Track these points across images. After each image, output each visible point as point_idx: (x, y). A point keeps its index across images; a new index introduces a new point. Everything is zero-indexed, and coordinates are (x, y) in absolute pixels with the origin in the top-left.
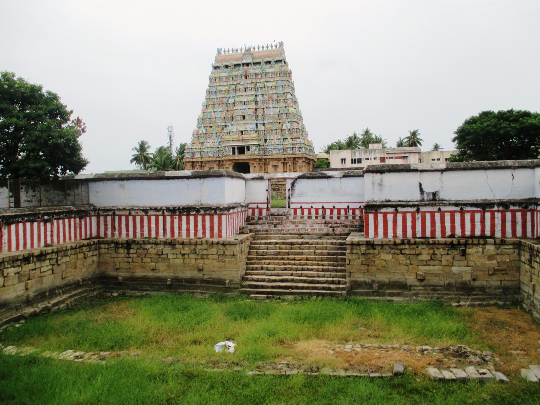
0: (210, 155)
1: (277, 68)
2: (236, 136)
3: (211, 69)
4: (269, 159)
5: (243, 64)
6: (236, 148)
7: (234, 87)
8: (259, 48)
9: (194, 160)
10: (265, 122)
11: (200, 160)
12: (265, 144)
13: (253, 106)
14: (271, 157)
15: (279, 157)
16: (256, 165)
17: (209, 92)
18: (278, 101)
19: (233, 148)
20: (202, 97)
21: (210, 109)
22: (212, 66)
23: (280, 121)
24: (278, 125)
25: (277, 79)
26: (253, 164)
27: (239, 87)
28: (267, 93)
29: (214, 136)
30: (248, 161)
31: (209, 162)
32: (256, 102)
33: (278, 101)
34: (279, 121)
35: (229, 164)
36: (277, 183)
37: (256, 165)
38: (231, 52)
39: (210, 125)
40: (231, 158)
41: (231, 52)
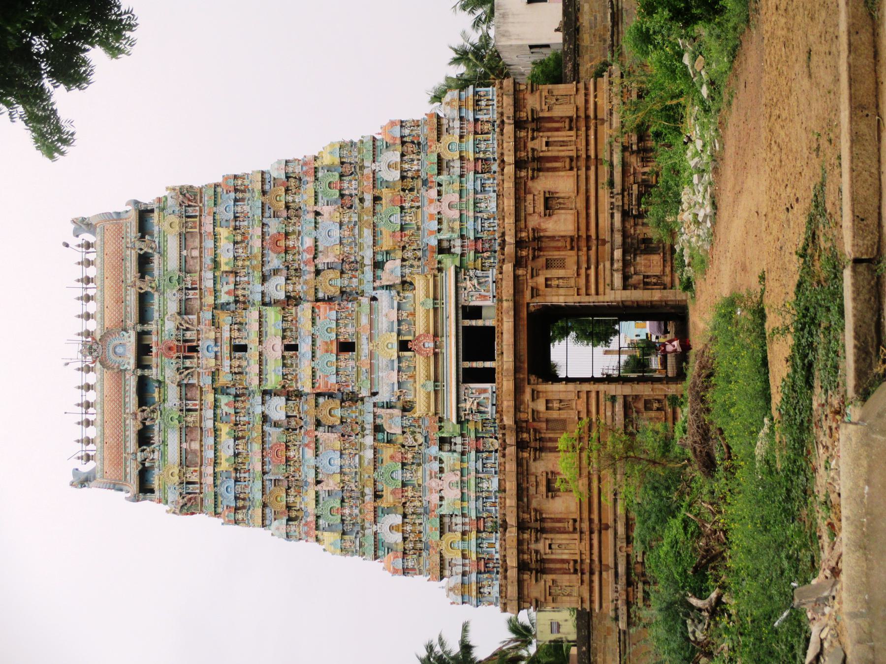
0: (494, 485)
1: (167, 229)
2: (420, 361)
3: (148, 506)
4: (517, 231)
5: (141, 364)
6: (468, 365)
7: (224, 400)
8: (88, 316)
9: (512, 562)
10: (368, 261)
11: (512, 533)
12: (458, 250)
13: (304, 311)
14: (510, 221)
15: (509, 185)
16: (541, 280)
17: (238, 511)
18: (292, 211)
19: (469, 376)
20: (259, 545)
21: (307, 502)
22: (137, 500)
23: (368, 197)
24: (385, 206)
25: (208, 221)
26: (535, 292)
27: (225, 378)
28: (256, 262)
29: (418, 476)
30: (524, 314)
31: (521, 492)
32: (292, 300)
33: (292, 211)
34: (368, 203)
35: (535, 395)
36: (618, 188)
37: (541, 280)
38: (92, 432)
39: (369, 497)
40: (507, 384)
41: (92, 432)
